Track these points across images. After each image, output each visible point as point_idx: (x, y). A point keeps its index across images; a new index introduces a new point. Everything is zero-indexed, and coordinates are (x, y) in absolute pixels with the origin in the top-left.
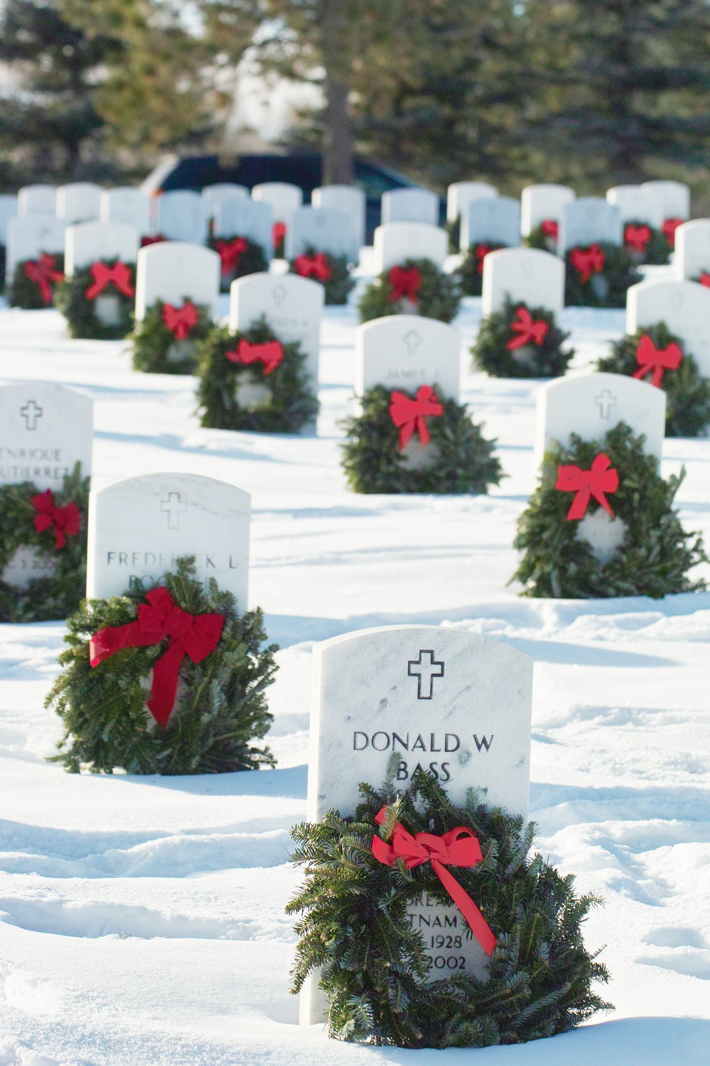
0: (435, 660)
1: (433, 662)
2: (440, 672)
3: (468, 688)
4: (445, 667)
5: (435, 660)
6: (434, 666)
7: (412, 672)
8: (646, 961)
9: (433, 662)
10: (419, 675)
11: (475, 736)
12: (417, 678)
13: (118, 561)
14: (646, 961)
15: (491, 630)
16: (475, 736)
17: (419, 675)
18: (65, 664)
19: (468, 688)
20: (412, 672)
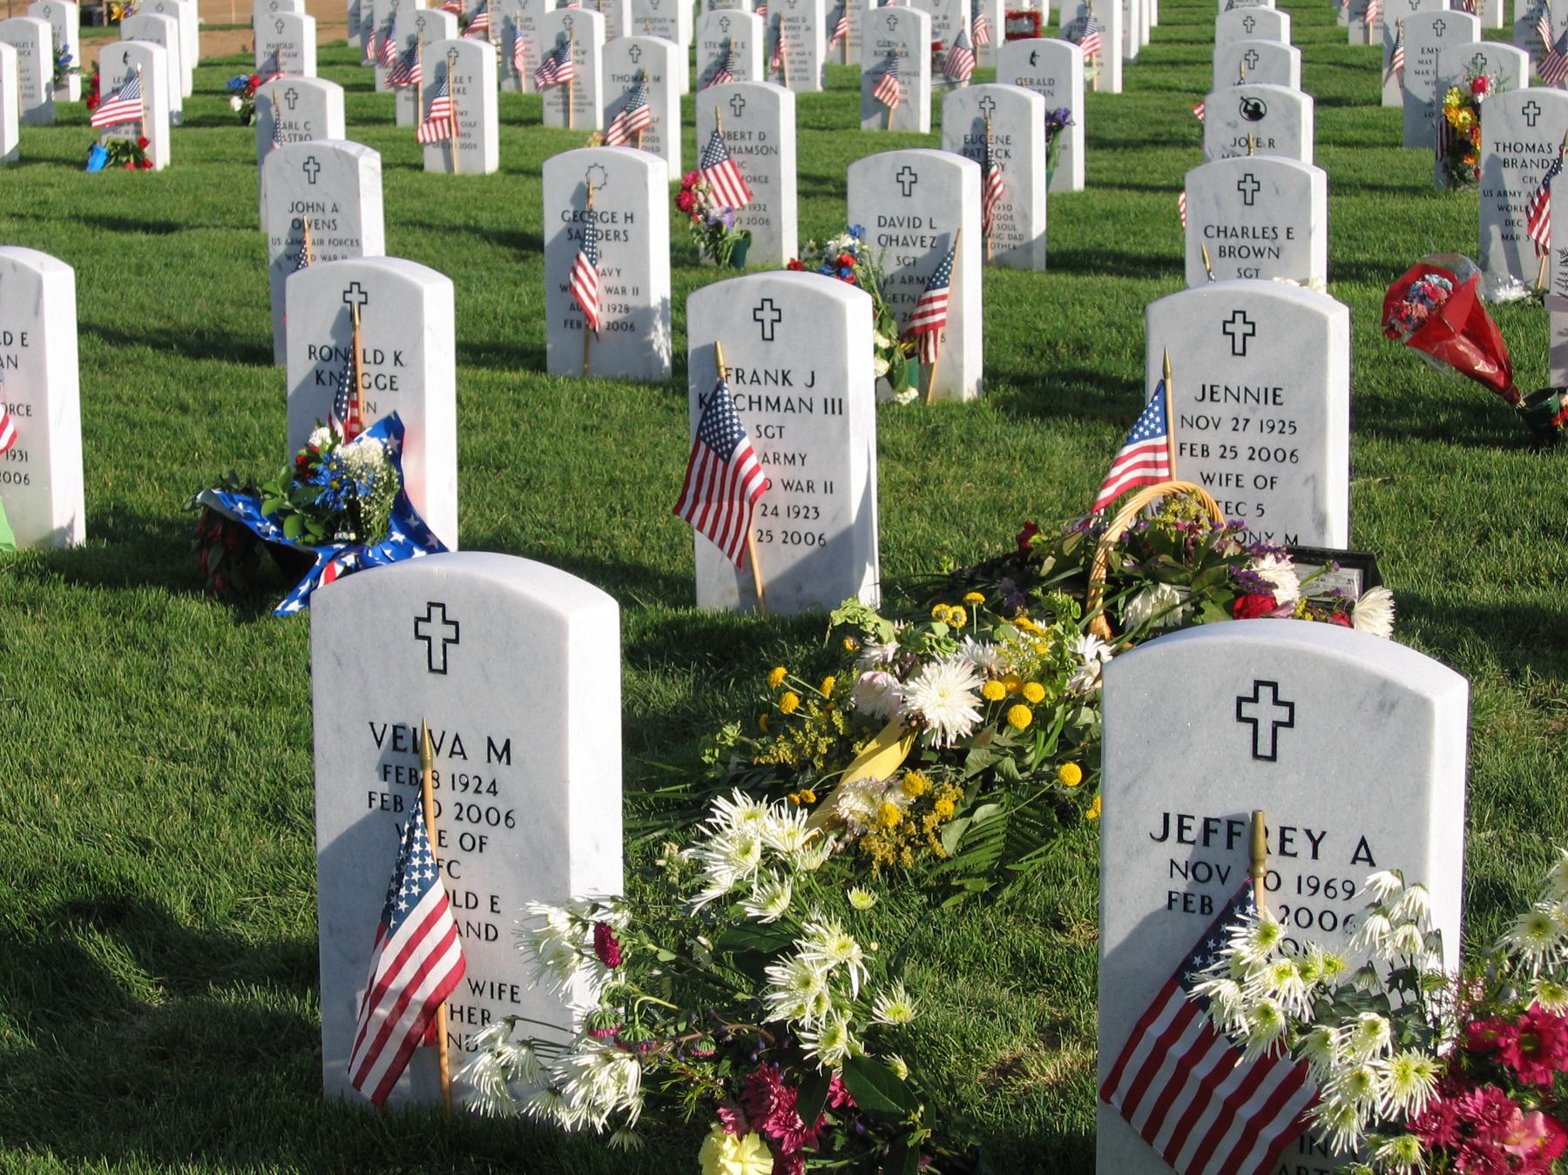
0: (1251, 695)
1: (1255, 699)
2: (1250, 726)
3: (339, 729)
4: (440, 676)
5: (1251, 695)
6: (1278, 708)
7: (1286, 710)
8: (1166, 816)
9: (1255, 699)
10: (1255, 722)
11: (509, 763)
12: (1250, 726)
13: (508, 1014)
14: (1166, 816)
15: (1373, 1120)
16: (509, 763)
17: (1255, 722)
18: (739, 237)
19: (339, 729)
20: (1286, 710)
